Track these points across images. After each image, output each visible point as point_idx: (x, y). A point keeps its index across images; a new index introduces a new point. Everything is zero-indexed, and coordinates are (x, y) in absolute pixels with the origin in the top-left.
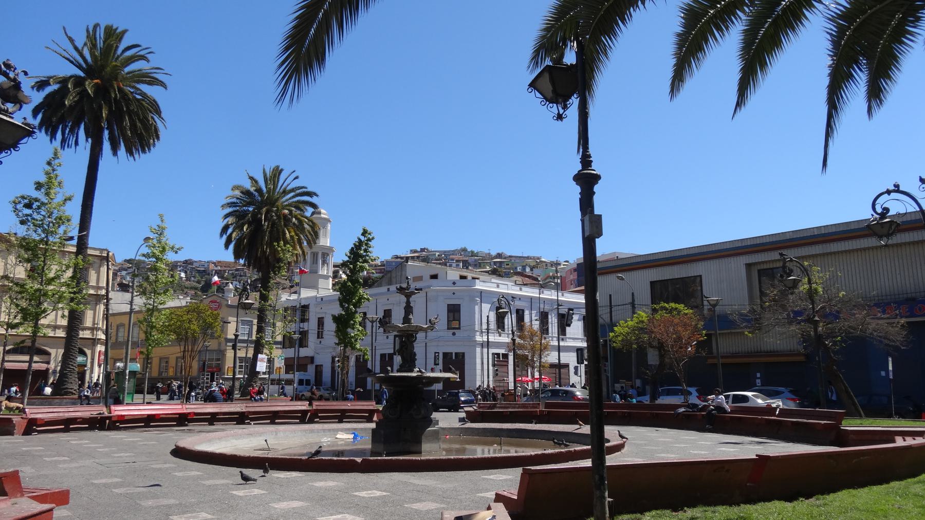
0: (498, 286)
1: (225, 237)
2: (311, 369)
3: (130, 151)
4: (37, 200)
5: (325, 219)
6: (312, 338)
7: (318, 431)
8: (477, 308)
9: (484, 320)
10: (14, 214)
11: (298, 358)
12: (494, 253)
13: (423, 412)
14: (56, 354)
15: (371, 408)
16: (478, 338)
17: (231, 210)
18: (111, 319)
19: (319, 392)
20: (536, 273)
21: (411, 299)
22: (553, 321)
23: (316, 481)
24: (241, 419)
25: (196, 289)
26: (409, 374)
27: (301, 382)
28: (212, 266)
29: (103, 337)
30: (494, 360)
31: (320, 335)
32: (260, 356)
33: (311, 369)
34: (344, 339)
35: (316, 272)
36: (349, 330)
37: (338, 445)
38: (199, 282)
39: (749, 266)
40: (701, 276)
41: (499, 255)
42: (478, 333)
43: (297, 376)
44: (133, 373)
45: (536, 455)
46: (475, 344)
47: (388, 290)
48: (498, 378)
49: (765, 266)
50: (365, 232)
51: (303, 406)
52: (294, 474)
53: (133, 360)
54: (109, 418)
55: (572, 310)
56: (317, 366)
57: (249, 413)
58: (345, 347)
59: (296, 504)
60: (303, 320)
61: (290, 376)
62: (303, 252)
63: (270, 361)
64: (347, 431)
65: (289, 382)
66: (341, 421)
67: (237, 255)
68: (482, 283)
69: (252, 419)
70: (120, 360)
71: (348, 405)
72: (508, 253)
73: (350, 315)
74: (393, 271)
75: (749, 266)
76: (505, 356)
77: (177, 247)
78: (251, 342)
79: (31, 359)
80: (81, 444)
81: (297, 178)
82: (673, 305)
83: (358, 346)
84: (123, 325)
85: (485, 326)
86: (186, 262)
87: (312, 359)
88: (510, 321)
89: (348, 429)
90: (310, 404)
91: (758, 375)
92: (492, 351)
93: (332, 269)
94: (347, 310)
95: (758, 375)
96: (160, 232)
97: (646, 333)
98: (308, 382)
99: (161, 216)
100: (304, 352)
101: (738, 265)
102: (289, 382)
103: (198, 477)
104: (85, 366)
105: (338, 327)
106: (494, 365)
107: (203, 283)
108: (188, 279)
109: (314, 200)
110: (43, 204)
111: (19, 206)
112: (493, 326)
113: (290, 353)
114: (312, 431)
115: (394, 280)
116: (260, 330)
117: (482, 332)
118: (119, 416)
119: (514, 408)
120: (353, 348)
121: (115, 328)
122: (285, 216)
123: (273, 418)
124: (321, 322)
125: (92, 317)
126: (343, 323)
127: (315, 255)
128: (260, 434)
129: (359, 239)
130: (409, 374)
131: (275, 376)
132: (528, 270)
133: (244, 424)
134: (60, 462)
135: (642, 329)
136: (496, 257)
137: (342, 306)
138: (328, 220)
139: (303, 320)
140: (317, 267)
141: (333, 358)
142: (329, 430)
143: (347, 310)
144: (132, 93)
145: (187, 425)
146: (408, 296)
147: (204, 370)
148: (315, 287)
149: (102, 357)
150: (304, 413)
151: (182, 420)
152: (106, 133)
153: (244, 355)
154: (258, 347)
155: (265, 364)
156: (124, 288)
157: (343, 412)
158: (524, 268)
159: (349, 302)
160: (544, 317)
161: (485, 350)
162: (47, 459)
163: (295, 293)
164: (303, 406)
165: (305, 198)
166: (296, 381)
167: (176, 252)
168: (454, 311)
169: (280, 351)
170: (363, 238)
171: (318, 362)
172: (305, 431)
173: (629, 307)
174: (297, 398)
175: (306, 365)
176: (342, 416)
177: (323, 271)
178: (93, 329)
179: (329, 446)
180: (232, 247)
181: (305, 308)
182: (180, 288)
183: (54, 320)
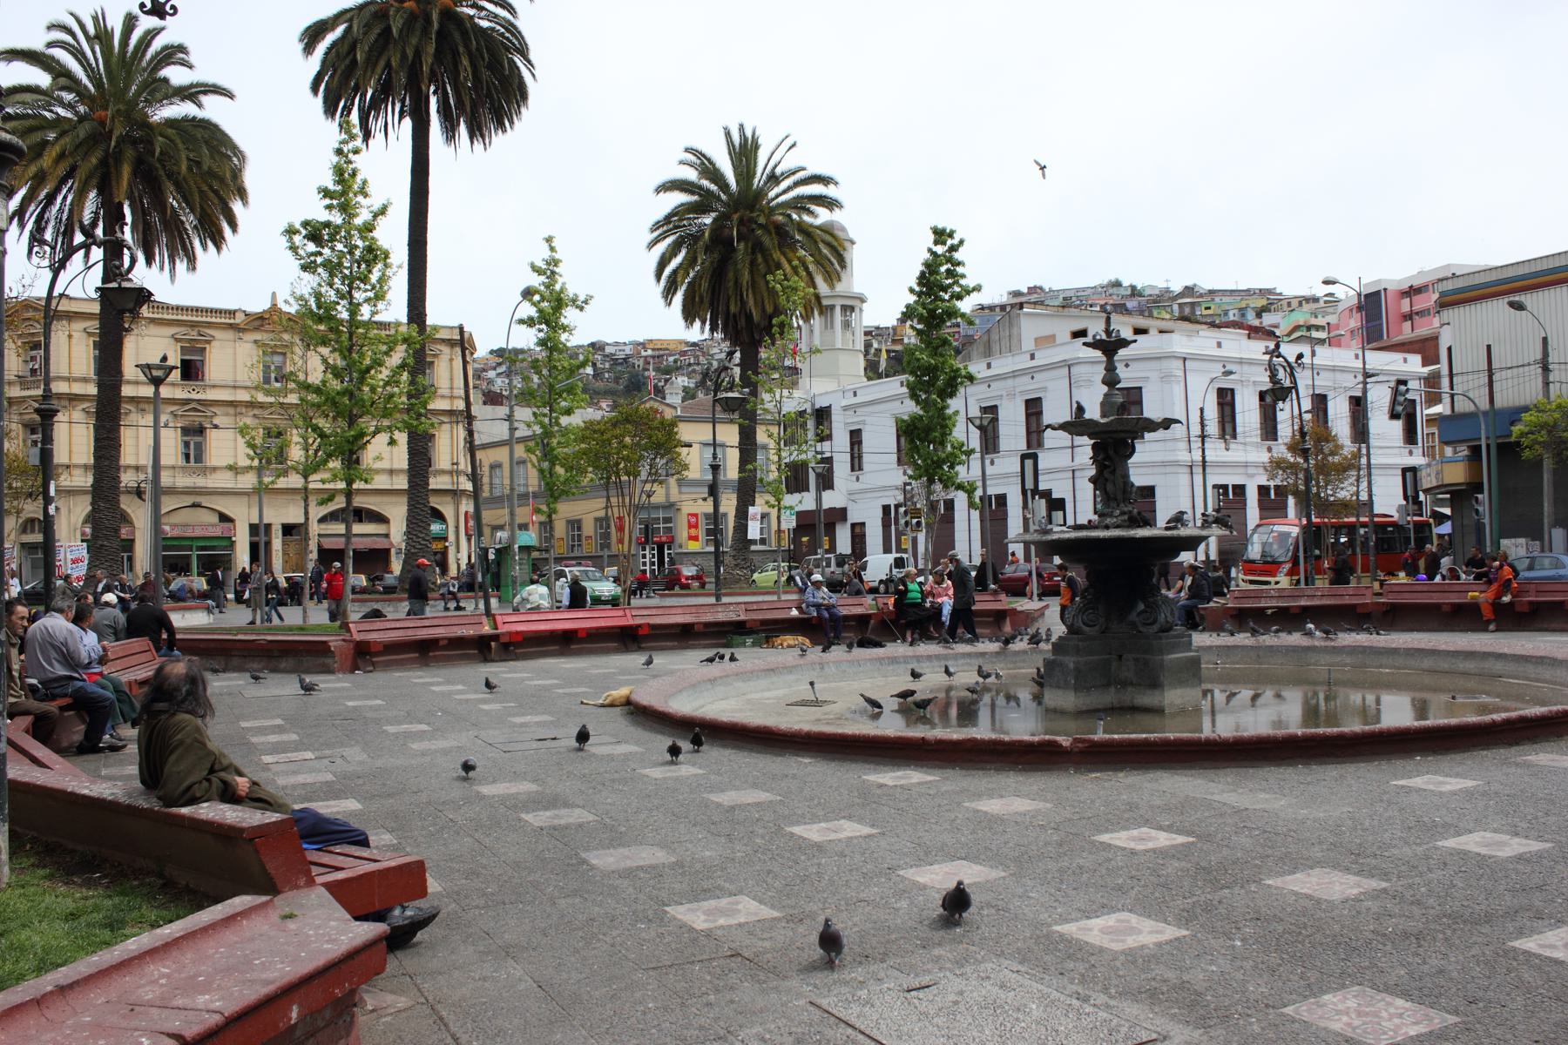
3: (476, 131)
4: (327, 224)
10: (289, 253)
12: (1177, 288)
14: (397, 513)
18: (479, 455)
20: (1268, 320)
23: (979, 796)
29: (469, 486)
31: (856, 463)
32: (751, 510)
41: (1189, 290)
44: (525, 549)
50: (940, 235)
53: (524, 527)
54: (495, 637)
60: (824, 437)
67: (689, 314)
70: (501, 528)
72: (1206, 284)
77: (582, 298)
79: (349, 529)
80: (451, 693)
84: (499, 466)
87: (840, 514)
92: (1214, 479)
96: (549, 270)
99: (549, 240)
100: (831, 500)
104: (446, 539)
109: (829, 191)
110: (337, 229)
111: (297, 239)
112: (1213, 428)
115: (995, 348)
118: (510, 634)
121: (486, 469)
125: (447, 447)
134: (409, 736)
137: (914, 396)
139: (824, 437)
143: (925, 405)
144: (472, 17)
149: (471, 523)
152: (433, 101)
156: (492, 399)
162: (391, 729)
165: (818, 190)
167: (581, 309)
170: (940, 249)
178: (454, 472)
180: (678, 298)
182: (594, 396)
183: (386, 455)
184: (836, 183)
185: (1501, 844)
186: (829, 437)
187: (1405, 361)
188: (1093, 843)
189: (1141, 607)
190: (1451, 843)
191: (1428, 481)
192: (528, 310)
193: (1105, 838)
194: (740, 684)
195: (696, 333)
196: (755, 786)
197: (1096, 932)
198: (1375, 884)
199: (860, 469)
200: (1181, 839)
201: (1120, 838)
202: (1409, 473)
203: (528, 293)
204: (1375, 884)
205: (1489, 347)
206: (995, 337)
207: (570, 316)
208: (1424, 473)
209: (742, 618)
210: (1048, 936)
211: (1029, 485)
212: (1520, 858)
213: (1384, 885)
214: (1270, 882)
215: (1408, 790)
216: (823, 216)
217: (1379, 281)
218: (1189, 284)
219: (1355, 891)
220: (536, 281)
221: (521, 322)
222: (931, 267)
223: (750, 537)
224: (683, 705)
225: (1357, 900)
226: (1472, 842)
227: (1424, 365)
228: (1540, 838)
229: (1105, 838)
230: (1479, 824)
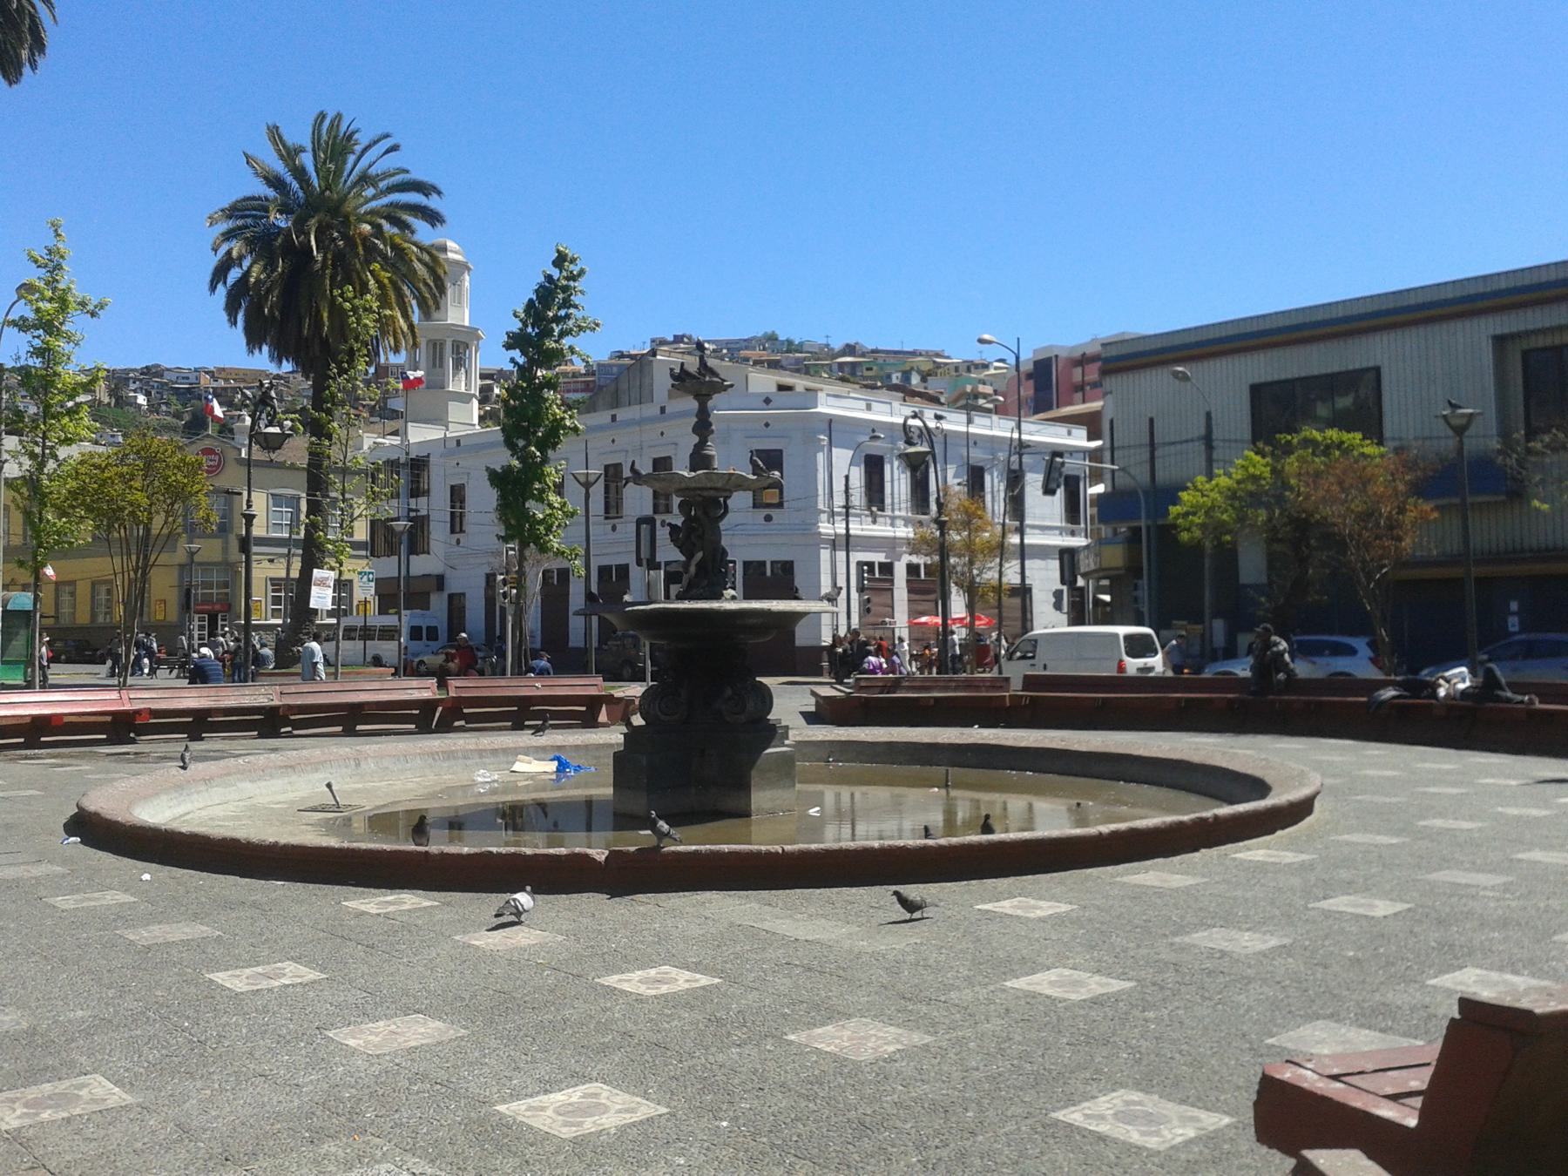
0: (869, 408)
1: (221, 290)
2: (439, 603)
5: (457, 263)
6: (438, 532)
7: (466, 754)
8: (821, 457)
9: (839, 486)
11: (408, 577)
12: (837, 345)
13: (750, 706)
15: (593, 692)
16: (825, 528)
17: (230, 224)
19: (461, 659)
20: (933, 387)
21: (710, 404)
22: (995, 485)
24: (269, 723)
25: (174, 429)
26: (715, 605)
27: (415, 633)
28: (205, 380)
30: (860, 578)
31: (457, 524)
32: (317, 573)
33: (439, 603)
34: (518, 524)
35: (442, 386)
36: (530, 504)
37: (516, 789)
38: (178, 415)
39: (1500, 341)
40: (1377, 370)
41: (850, 349)
42: (824, 517)
43: (405, 619)
45: (1114, 834)
46: (817, 540)
47: (614, 418)
48: (871, 619)
49: (1541, 342)
50: (560, 260)
51: (422, 690)
52: (409, 900)
55: (1060, 455)
56: (451, 596)
57: (290, 707)
58: (524, 545)
59: (420, 1031)
60: (416, 491)
61: (390, 620)
62: (411, 326)
63: (342, 586)
64: (539, 753)
65: (389, 634)
66: (518, 726)
68: (831, 401)
69: (297, 725)
71: (536, 687)
73: (532, 470)
74: (618, 383)
75: (1500, 341)
76: (887, 568)
78: (297, 543)
81: (394, 148)
82: (1333, 434)
83: (555, 543)
85: (839, 500)
86: (147, 371)
87: (439, 582)
88: (898, 482)
89: (544, 749)
90: (442, 685)
91: (1514, 606)
92: (858, 556)
93: (476, 384)
94: (525, 457)
95: (1514, 606)
96: (53, 264)
97: (1260, 504)
98: (432, 633)
100: (421, 565)
101: (1475, 338)
102: (389, 634)
103: (123, 916)
105: (502, 497)
106: (861, 589)
107: (187, 417)
108: (153, 408)
109: (433, 202)
112: (858, 498)
113: (389, 566)
114: (450, 755)
116: (314, 508)
117: (833, 514)
119: (946, 689)
120: (543, 548)
122: (365, 239)
123: (351, 720)
124: (457, 495)
126: (515, 488)
127: (436, 348)
128: (316, 766)
129: (549, 278)
130: (715, 605)
131: (355, 620)
132: (915, 380)
133: (278, 735)
135: (1251, 494)
136: (843, 353)
137: (509, 443)
138: (464, 267)
139: (416, 491)
140: (444, 375)
141: (490, 578)
142: (494, 752)
143: (525, 457)
145: (133, 741)
146: (703, 397)
147: (188, 607)
148: (440, 419)
150: (427, 706)
151: (121, 728)
153: (283, 574)
154: (313, 553)
155: (330, 593)
157: (525, 703)
158: (906, 376)
159: (526, 434)
160: (975, 478)
161: (841, 555)
163: (395, 433)
164: (422, 690)
165: (417, 200)
166: (405, 631)
167: (93, 314)
168: (771, 459)
169: (361, 565)
170: (555, 273)
171: (453, 586)
172: (433, 755)
173: (1200, 447)
174: (409, 669)
175: (428, 594)
176: (522, 715)
177: (457, 384)
179: (494, 792)
181: (418, 465)
184: (439, 193)
185: (1077, 984)
186: (427, 493)
187: (1069, 433)
188: (594, 987)
189: (729, 692)
190: (1021, 983)
191: (1086, 563)
192: (24, 310)
193: (612, 980)
194: (247, 785)
195: (262, 361)
196: (196, 917)
197: (549, 1112)
198: (918, 1038)
199: (462, 531)
200: (704, 980)
201: (632, 982)
202: (1068, 558)
203: (26, 289)
204: (918, 1038)
205: (1151, 420)
206: (624, 386)
207: (75, 323)
208: (1082, 556)
209: (276, 702)
210: (481, 1122)
211: (645, 554)
212: (1096, 1002)
213: (928, 1039)
214: (792, 1037)
215: (990, 916)
216: (423, 232)
217: (1051, 347)
218: (852, 342)
219: (891, 1049)
220: (35, 276)
221: (14, 323)
222: (265, 178)
223: (312, 605)
224: (157, 812)
225: (891, 1060)
226: (1043, 982)
227: (1089, 439)
228: (1122, 976)
229: (612, 980)
230: (1061, 960)
